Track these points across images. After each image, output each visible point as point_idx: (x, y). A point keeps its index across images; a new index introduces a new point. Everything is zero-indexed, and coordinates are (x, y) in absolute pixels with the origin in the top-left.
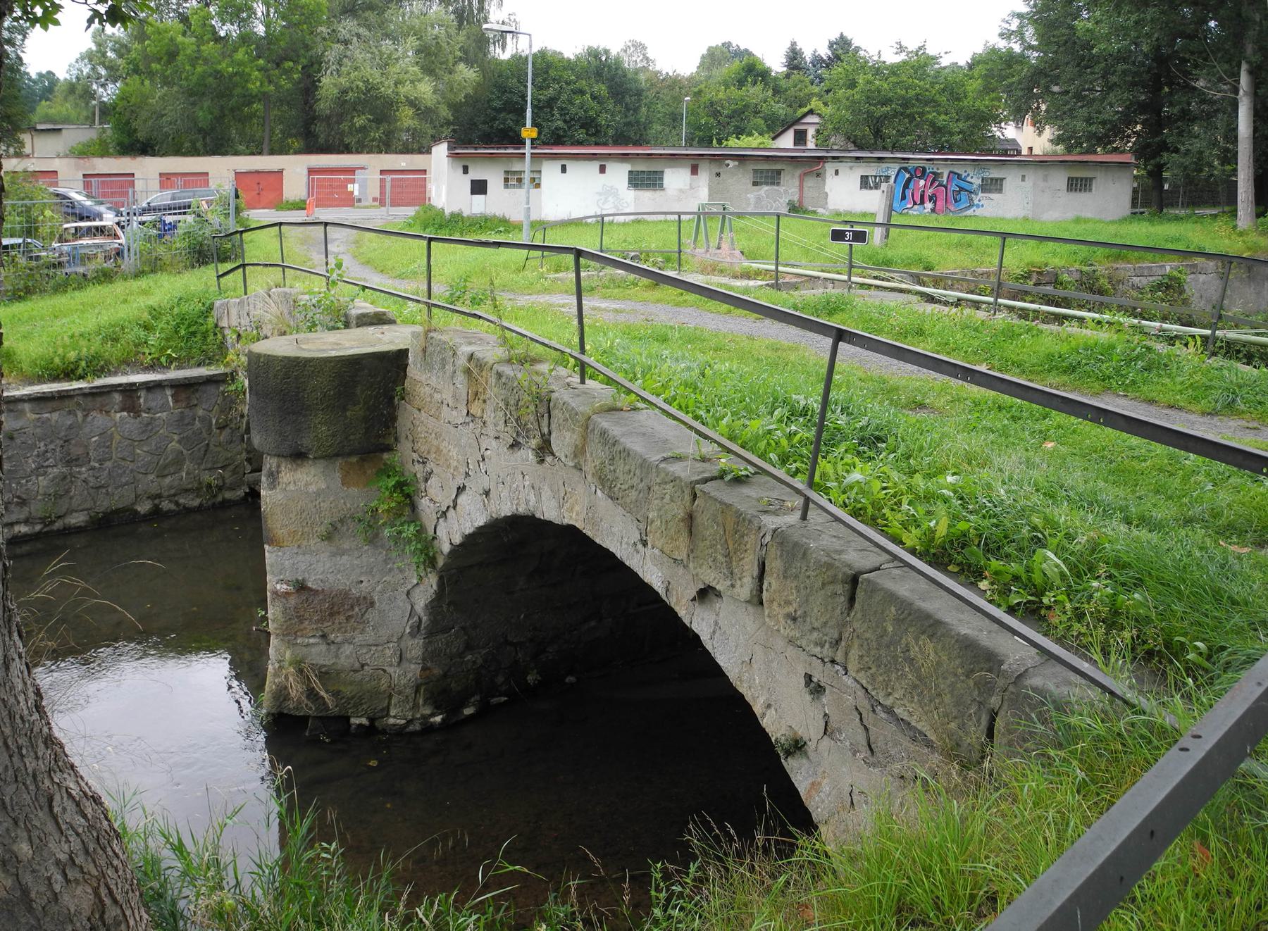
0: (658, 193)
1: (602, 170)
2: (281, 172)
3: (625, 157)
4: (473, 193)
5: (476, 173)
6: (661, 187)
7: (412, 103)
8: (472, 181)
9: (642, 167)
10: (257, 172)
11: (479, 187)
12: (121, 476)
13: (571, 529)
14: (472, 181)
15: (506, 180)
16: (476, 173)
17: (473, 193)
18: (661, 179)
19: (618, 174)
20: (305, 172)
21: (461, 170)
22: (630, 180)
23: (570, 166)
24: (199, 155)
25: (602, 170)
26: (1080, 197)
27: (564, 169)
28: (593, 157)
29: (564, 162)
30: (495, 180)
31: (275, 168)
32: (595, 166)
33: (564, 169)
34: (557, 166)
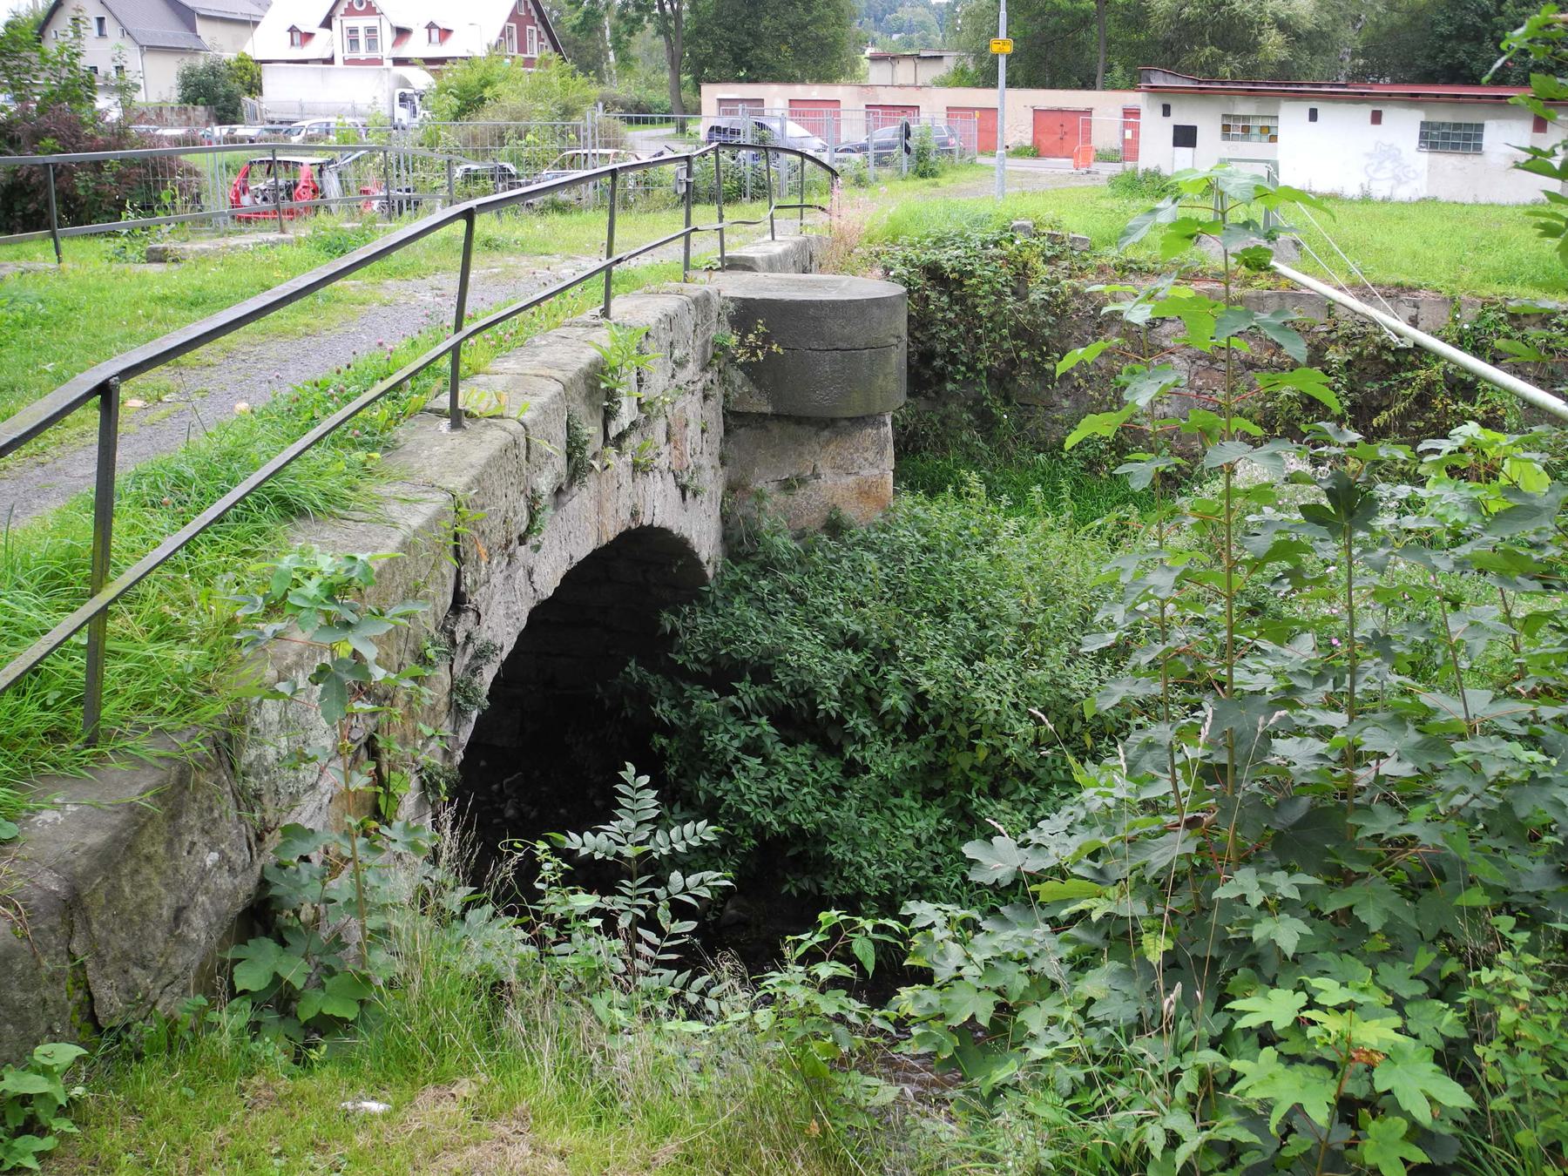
0: (1477, 159)
1: (1376, 118)
2: (1089, 112)
3: (1413, 100)
4: (1176, 144)
5: (1183, 115)
6: (1478, 148)
7: (1282, 25)
8: (1176, 127)
9: (1444, 116)
10: (1060, 111)
11: (1185, 137)
12: (918, 869)
13: (533, 613)
14: (1176, 127)
15: (1226, 128)
16: (1181, 117)
17: (1176, 144)
18: (1480, 137)
19: (1404, 125)
20: (1120, 113)
21: (1160, 111)
22: (1423, 137)
23: (1324, 110)
24: (1115, 88)
25: (1376, 118)
26: (1449, 162)
27: (1313, 115)
28: (1360, 98)
29: (1314, 105)
30: (1208, 125)
31: (1082, 106)
32: (1366, 111)
33: (1313, 115)
34: (1303, 109)
